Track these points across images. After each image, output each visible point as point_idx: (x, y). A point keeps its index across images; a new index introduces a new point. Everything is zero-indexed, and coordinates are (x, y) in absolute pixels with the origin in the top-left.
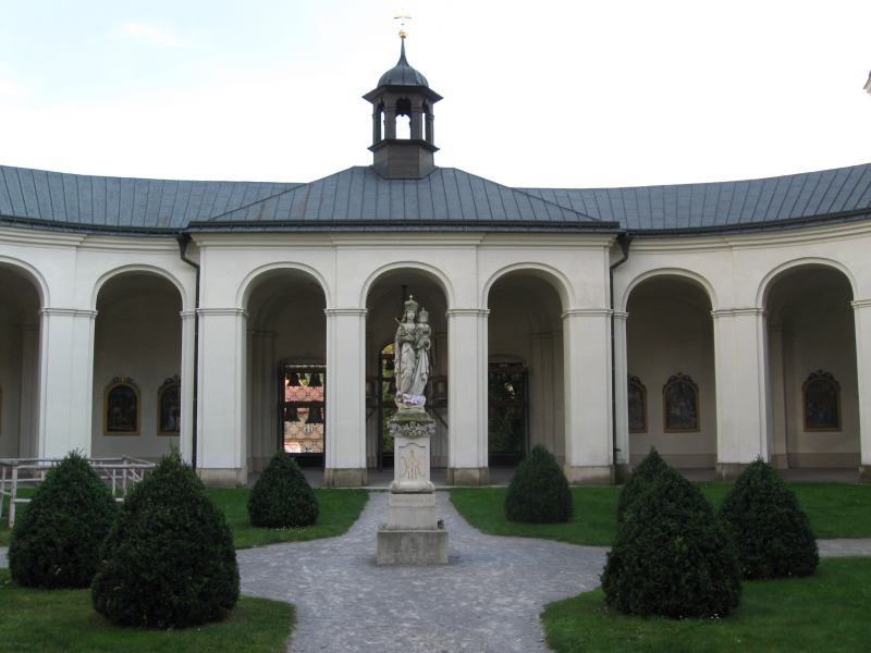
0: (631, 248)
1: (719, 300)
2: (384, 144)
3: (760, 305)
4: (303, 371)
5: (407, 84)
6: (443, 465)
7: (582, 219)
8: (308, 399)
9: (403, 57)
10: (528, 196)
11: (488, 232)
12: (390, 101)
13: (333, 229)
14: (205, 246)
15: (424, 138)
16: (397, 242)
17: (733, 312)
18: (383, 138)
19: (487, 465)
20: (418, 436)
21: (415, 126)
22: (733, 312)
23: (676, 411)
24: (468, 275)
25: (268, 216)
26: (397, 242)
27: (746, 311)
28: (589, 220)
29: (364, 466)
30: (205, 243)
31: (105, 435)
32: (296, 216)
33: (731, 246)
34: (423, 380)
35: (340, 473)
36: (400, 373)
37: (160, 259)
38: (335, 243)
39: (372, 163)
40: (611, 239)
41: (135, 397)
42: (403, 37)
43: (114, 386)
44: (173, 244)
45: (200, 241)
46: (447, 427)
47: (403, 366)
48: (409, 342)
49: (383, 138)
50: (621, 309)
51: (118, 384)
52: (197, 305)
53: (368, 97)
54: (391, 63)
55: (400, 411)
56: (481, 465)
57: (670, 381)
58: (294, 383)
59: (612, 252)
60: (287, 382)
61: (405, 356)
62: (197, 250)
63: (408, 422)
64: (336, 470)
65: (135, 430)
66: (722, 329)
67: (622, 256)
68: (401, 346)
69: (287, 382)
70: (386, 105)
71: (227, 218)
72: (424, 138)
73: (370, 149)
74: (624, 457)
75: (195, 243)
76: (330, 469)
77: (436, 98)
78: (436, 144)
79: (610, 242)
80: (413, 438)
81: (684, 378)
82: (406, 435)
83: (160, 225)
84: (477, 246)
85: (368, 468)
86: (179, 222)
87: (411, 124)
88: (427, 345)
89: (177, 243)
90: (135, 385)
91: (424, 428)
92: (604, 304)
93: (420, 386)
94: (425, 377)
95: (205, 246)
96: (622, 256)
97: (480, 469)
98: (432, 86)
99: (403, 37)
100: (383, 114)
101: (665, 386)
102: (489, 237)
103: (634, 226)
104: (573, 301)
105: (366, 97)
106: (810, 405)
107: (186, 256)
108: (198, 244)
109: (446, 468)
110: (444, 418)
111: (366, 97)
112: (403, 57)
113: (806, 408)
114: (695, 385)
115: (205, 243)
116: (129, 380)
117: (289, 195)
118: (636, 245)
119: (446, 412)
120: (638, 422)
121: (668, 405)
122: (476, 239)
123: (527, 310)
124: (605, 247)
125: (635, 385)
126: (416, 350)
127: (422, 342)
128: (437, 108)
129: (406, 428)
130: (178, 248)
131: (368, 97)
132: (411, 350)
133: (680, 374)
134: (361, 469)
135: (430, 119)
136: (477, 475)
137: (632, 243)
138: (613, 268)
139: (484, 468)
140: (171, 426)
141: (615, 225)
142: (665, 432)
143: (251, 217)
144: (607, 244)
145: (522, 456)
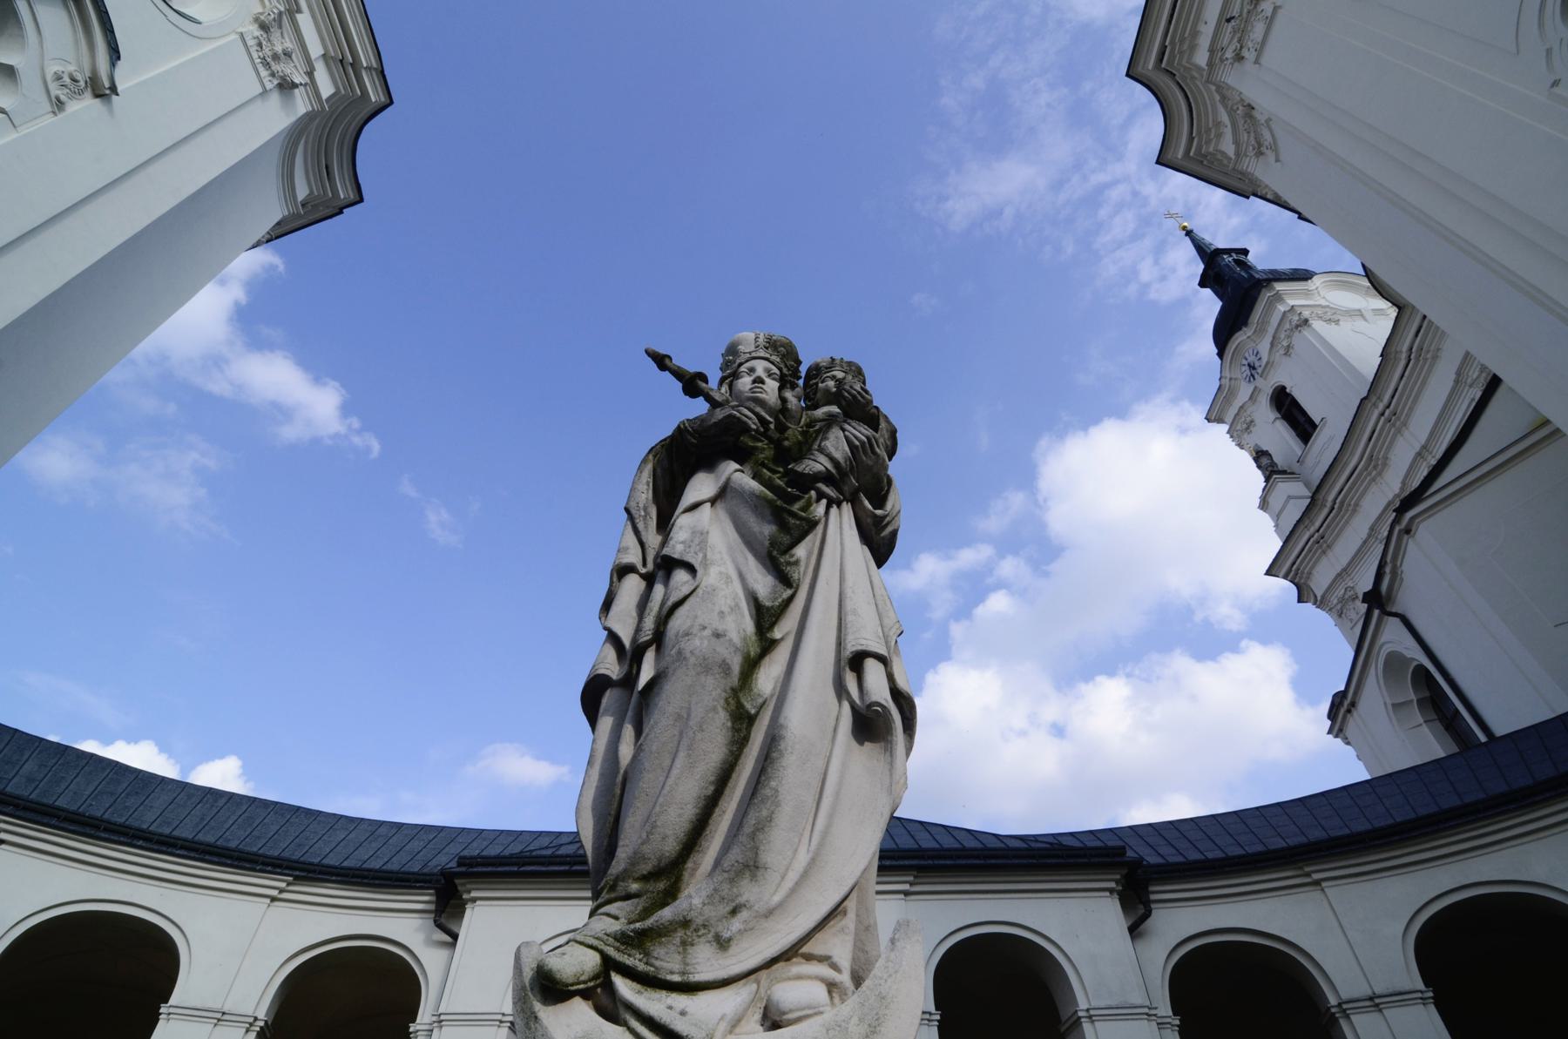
30: (474, 894)
79: (1117, 882)
84: (906, 893)
95: (474, 900)
115: (474, 894)
144: (1113, 885)
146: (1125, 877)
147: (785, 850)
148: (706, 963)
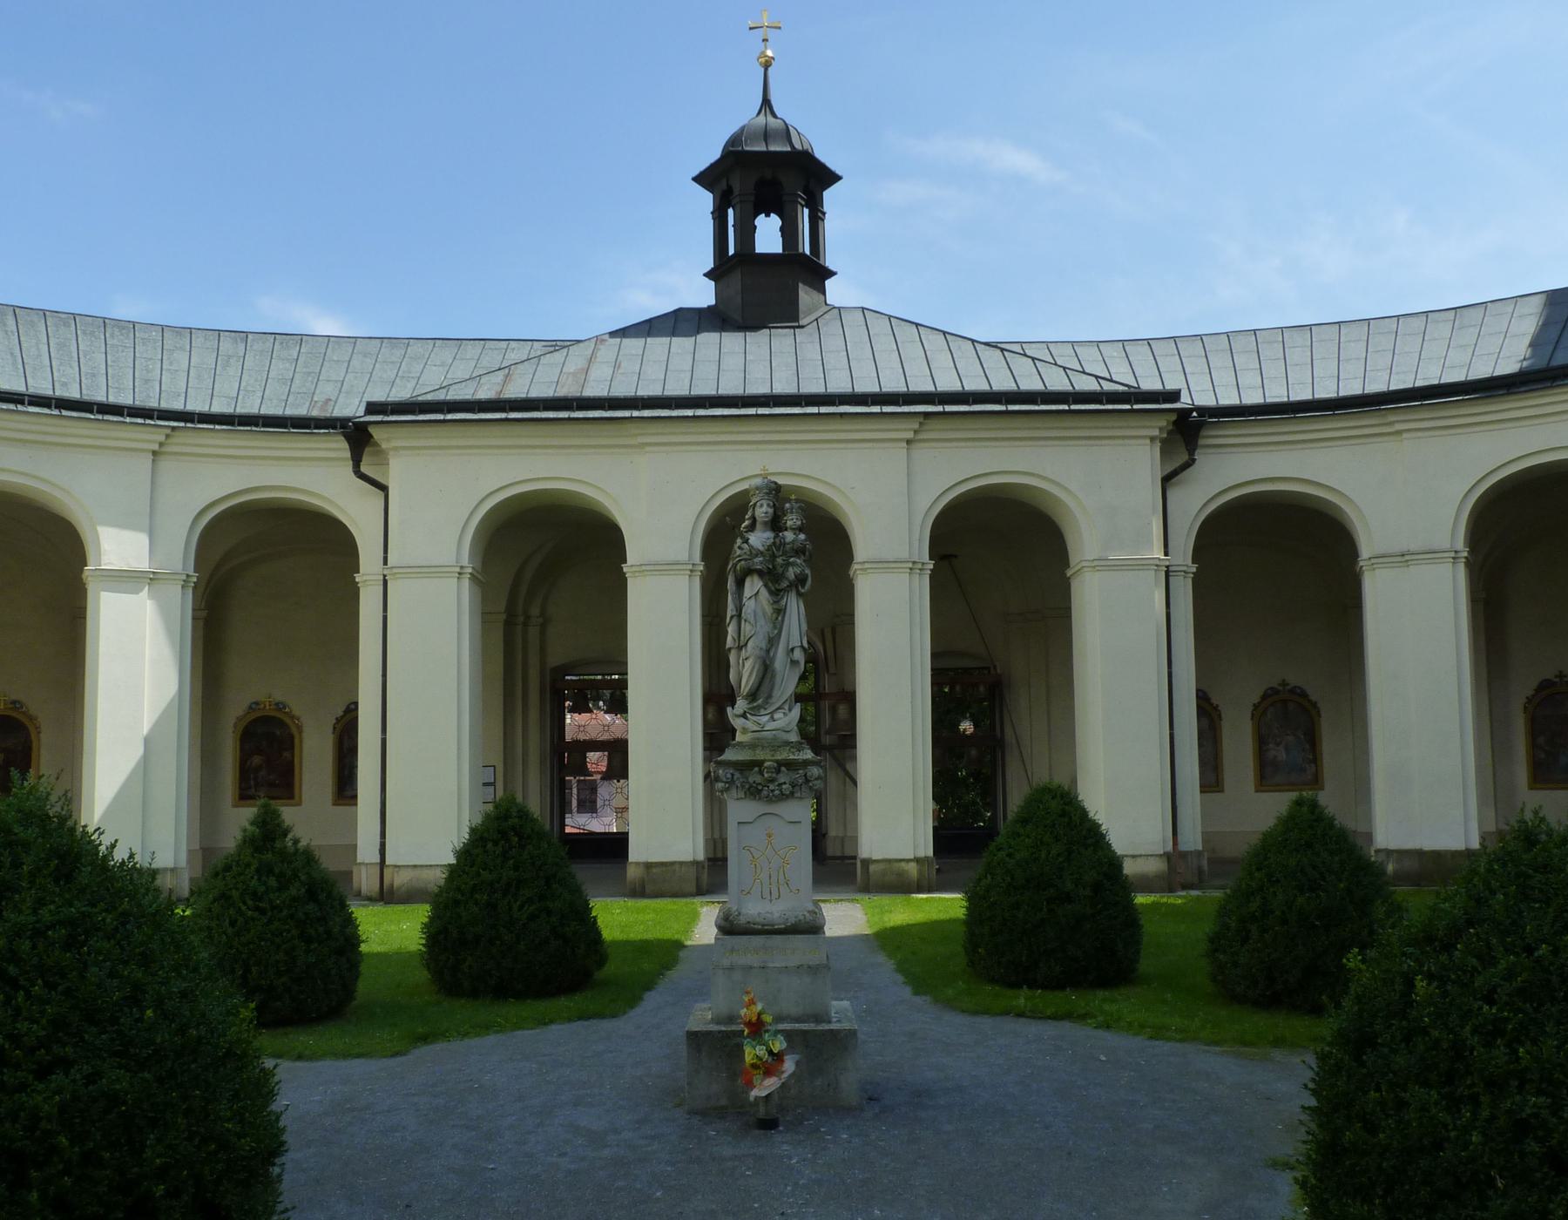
0: (1201, 442)
1: (1373, 536)
2: (734, 265)
3: (1460, 544)
4: (595, 686)
5: (772, 148)
6: (848, 852)
7: (1108, 386)
8: (605, 737)
9: (766, 103)
10: (1002, 350)
11: (927, 415)
13: (636, 413)
14: (396, 449)
15: (807, 251)
16: (759, 437)
17: (1404, 558)
18: (731, 251)
19: (930, 853)
20: (783, 797)
22: (1404, 558)
23: (1278, 753)
24: (887, 504)
25: (515, 391)
26: (759, 437)
27: (1431, 554)
28: (1121, 388)
29: (701, 857)
30: (394, 444)
31: (299, 804)
32: (568, 390)
33: (1399, 433)
34: (794, 663)
36: (740, 648)
37: (318, 478)
38: (640, 440)
39: (713, 302)
41: (292, 737)
42: (767, 66)
43: (253, 716)
44: (339, 447)
45: (388, 440)
46: (855, 783)
47: (747, 628)
48: (760, 573)
49: (731, 251)
50: (1183, 554)
51: (259, 714)
52: (385, 562)
53: (703, 179)
54: (741, 113)
55: (739, 737)
56: (921, 854)
57: (1264, 697)
59: (1165, 452)
61: (749, 606)
62: (382, 457)
63: (759, 764)
64: (648, 866)
65: (291, 797)
66: (1382, 594)
67: (1186, 457)
68: (740, 583)
70: (736, 191)
71: (441, 396)
73: (708, 275)
74: (1192, 840)
75: (376, 444)
76: (637, 864)
77: (831, 178)
78: (830, 262)
79: (1161, 429)
80: (770, 800)
81: (1293, 691)
82: (754, 792)
83: (315, 413)
84: (909, 442)
85: (709, 860)
86: (351, 408)
87: (782, 229)
90: (293, 718)
91: (798, 776)
93: (787, 683)
94: (798, 655)
96: (1186, 457)
97: (917, 860)
98: (821, 154)
99: (767, 66)
100: (731, 211)
101: (1256, 706)
102: (933, 424)
103: (1205, 399)
104: (1087, 542)
105: (695, 179)
106: (1541, 740)
107: (364, 469)
108: (384, 446)
109: (855, 858)
110: (848, 767)
111: (695, 179)
112: (766, 103)
113: (1533, 745)
114: (1315, 705)
115: (394, 444)
116: (280, 706)
117: (559, 357)
118: (1209, 437)
119: (854, 758)
120: (1212, 779)
121: (1261, 742)
122: (905, 430)
123: (999, 560)
124: (1152, 439)
125: (1207, 711)
126: (776, 594)
127: (791, 573)
128: (830, 196)
129: (754, 777)
130: (348, 454)
131: (703, 179)
132: (764, 592)
133: (1284, 683)
134: (695, 863)
135: (817, 218)
136: (913, 869)
137: (1204, 433)
138: (1167, 480)
139: (927, 858)
140: (348, 793)
141: (1174, 396)
142: (1531, 788)
143: (484, 394)
144: (1156, 432)
145: (991, 832)
146: (1175, 423)
147: (776, 693)
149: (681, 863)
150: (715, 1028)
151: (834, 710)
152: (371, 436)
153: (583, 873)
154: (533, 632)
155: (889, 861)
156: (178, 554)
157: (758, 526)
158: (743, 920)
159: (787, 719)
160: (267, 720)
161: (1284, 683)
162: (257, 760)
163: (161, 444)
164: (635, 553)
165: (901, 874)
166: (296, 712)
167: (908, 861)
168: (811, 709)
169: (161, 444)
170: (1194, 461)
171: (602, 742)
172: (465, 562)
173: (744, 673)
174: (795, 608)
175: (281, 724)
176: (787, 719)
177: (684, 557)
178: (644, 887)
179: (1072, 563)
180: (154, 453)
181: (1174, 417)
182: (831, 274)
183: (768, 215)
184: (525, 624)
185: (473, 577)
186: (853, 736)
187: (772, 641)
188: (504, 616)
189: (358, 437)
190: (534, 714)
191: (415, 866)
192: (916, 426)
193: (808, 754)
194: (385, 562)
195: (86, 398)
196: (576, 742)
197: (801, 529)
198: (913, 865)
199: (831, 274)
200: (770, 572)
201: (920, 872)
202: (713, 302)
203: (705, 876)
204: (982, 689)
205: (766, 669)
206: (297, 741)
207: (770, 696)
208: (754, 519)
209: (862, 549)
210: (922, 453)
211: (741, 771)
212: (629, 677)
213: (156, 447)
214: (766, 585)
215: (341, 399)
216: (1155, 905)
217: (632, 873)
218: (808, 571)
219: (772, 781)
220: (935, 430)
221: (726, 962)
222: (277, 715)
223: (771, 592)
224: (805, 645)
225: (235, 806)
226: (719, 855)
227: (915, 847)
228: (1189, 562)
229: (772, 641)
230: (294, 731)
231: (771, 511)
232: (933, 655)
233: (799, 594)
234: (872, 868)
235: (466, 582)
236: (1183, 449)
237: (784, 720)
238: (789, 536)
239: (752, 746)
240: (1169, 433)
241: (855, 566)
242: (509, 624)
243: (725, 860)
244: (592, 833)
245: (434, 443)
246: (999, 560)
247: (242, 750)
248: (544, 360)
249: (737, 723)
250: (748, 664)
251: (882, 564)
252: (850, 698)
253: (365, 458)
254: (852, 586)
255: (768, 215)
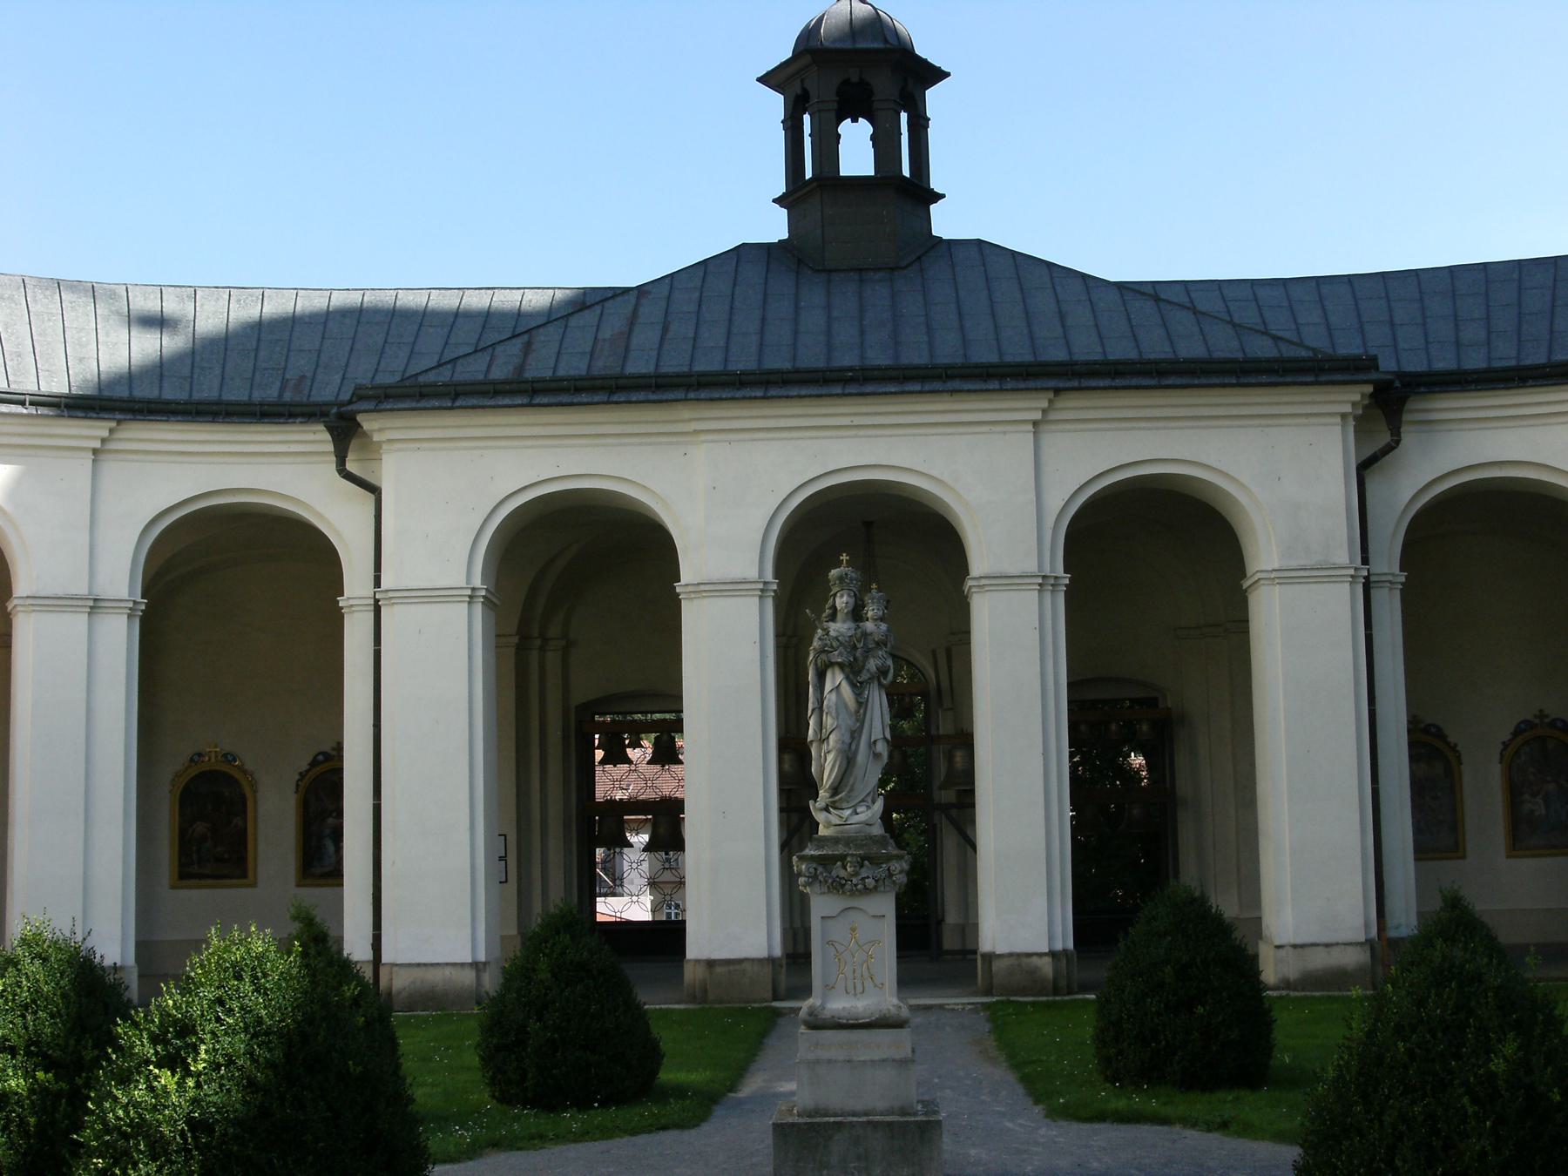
0: (1406, 417)
2: (811, 190)
6: (969, 947)
12: (824, 88)
15: (906, 172)
16: (845, 421)
18: (808, 174)
19: (1070, 945)
20: (867, 891)
21: (884, 144)
26: (845, 421)
28: (1304, 353)
29: (778, 952)
31: (254, 885)
34: (877, 756)
35: (719, 970)
36: (822, 741)
37: (285, 471)
39: (785, 236)
40: (1357, 397)
43: (193, 772)
47: (829, 722)
48: (841, 666)
49: (808, 174)
50: (1388, 561)
56: (1059, 946)
57: (1517, 732)
58: (616, 756)
59: (1362, 424)
60: (599, 754)
61: (830, 699)
62: (372, 451)
64: (711, 964)
65: (245, 876)
67: (1385, 438)
68: (821, 676)
69: (599, 754)
70: (814, 100)
72: (906, 172)
75: (365, 434)
76: (698, 961)
77: (937, 75)
79: (1354, 404)
80: (854, 893)
81: (1553, 724)
82: (837, 886)
84: (1035, 423)
87: (873, 138)
88: (883, 672)
89: (328, 437)
90: (245, 772)
91: (881, 871)
92: (1342, 552)
93: (869, 773)
94: (881, 748)
96: (1385, 438)
97: (1053, 954)
98: (924, 49)
100: (807, 118)
101: (1506, 745)
107: (351, 467)
109: (975, 952)
110: (969, 832)
116: (228, 758)
121: (1514, 793)
122: (1030, 406)
123: (1152, 566)
124: (1344, 416)
128: (935, 98)
129: (837, 871)
130: (331, 448)
133: (1542, 715)
134: (771, 960)
135: (919, 125)
136: (1046, 967)
137: (1410, 405)
138: (1364, 468)
139: (1065, 951)
144: (1348, 409)
146: (1372, 396)
148: (844, 805)
149: (753, 960)
150: (801, 1120)
151: (950, 759)
152: (359, 425)
153: (633, 970)
154: (553, 659)
155: (1019, 955)
156: (119, 577)
157: (839, 616)
158: (827, 1014)
159: (869, 813)
160: (210, 777)
161: (1542, 715)
162: (200, 828)
163: (103, 441)
164: (690, 571)
165: (1033, 971)
166: (249, 766)
167: (1040, 955)
168: (933, 732)
169: (103, 441)
170: (1398, 442)
171: (645, 802)
172: (477, 582)
173: (826, 765)
174: (878, 702)
175: (230, 781)
176: (869, 813)
177: (753, 573)
178: (705, 991)
179: (1249, 574)
180: (95, 451)
181: (1369, 389)
182: (938, 197)
183: (855, 120)
184: (542, 649)
185: (487, 602)
186: (971, 792)
187: (855, 734)
188: (515, 640)
189: (345, 432)
190: (555, 766)
191: (419, 965)
192: (1045, 404)
193: (892, 849)
194: (377, 583)
195: (14, 387)
196: (611, 803)
197: (882, 619)
198: (1048, 960)
199: (938, 197)
200: (851, 665)
201: (1056, 971)
202: (785, 236)
203: (783, 977)
204: (1145, 727)
205: (848, 760)
206: (250, 804)
207: (852, 790)
208: (834, 607)
209: (980, 562)
210: (1058, 442)
211: (824, 866)
212: (686, 716)
213: (97, 444)
214: (847, 678)
215: (319, 377)
216: (1281, 998)
217: (689, 973)
218: (890, 662)
219: (856, 874)
220: (1072, 406)
221: (811, 1056)
222: (224, 768)
223: (853, 685)
224: (888, 736)
225: (173, 887)
226: (801, 950)
227: (1051, 938)
228: (1396, 569)
229: (855, 734)
230: (248, 794)
231: (852, 600)
232: (1070, 685)
233: (880, 684)
234: (997, 966)
235: (478, 609)
236: (1384, 427)
237: (866, 815)
238: (869, 626)
239: (835, 840)
240: (1365, 407)
241: (970, 583)
242: (522, 649)
243: (807, 956)
244: (629, 922)
245: (439, 433)
246: (1152, 566)
247: (182, 815)
248: (573, 321)
249: (820, 817)
250: (830, 757)
251: (1003, 581)
252: (965, 740)
253: (350, 457)
254: (968, 605)
255: (855, 120)
